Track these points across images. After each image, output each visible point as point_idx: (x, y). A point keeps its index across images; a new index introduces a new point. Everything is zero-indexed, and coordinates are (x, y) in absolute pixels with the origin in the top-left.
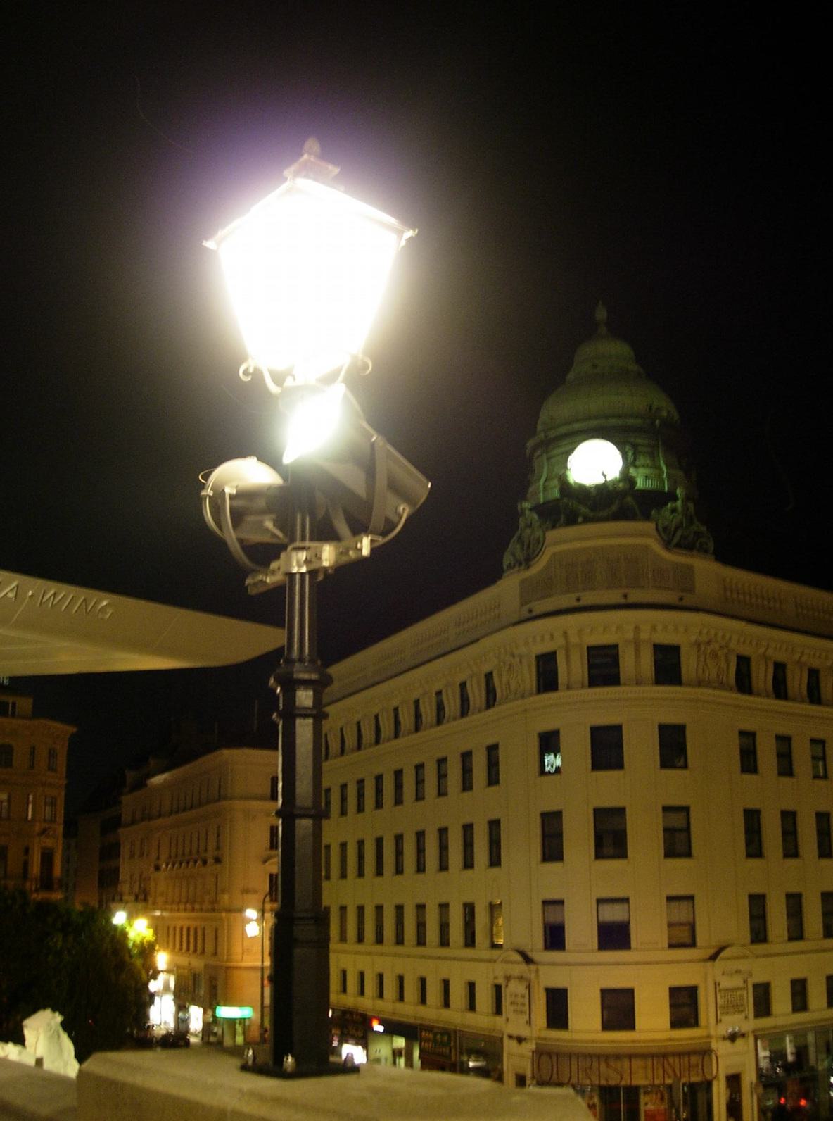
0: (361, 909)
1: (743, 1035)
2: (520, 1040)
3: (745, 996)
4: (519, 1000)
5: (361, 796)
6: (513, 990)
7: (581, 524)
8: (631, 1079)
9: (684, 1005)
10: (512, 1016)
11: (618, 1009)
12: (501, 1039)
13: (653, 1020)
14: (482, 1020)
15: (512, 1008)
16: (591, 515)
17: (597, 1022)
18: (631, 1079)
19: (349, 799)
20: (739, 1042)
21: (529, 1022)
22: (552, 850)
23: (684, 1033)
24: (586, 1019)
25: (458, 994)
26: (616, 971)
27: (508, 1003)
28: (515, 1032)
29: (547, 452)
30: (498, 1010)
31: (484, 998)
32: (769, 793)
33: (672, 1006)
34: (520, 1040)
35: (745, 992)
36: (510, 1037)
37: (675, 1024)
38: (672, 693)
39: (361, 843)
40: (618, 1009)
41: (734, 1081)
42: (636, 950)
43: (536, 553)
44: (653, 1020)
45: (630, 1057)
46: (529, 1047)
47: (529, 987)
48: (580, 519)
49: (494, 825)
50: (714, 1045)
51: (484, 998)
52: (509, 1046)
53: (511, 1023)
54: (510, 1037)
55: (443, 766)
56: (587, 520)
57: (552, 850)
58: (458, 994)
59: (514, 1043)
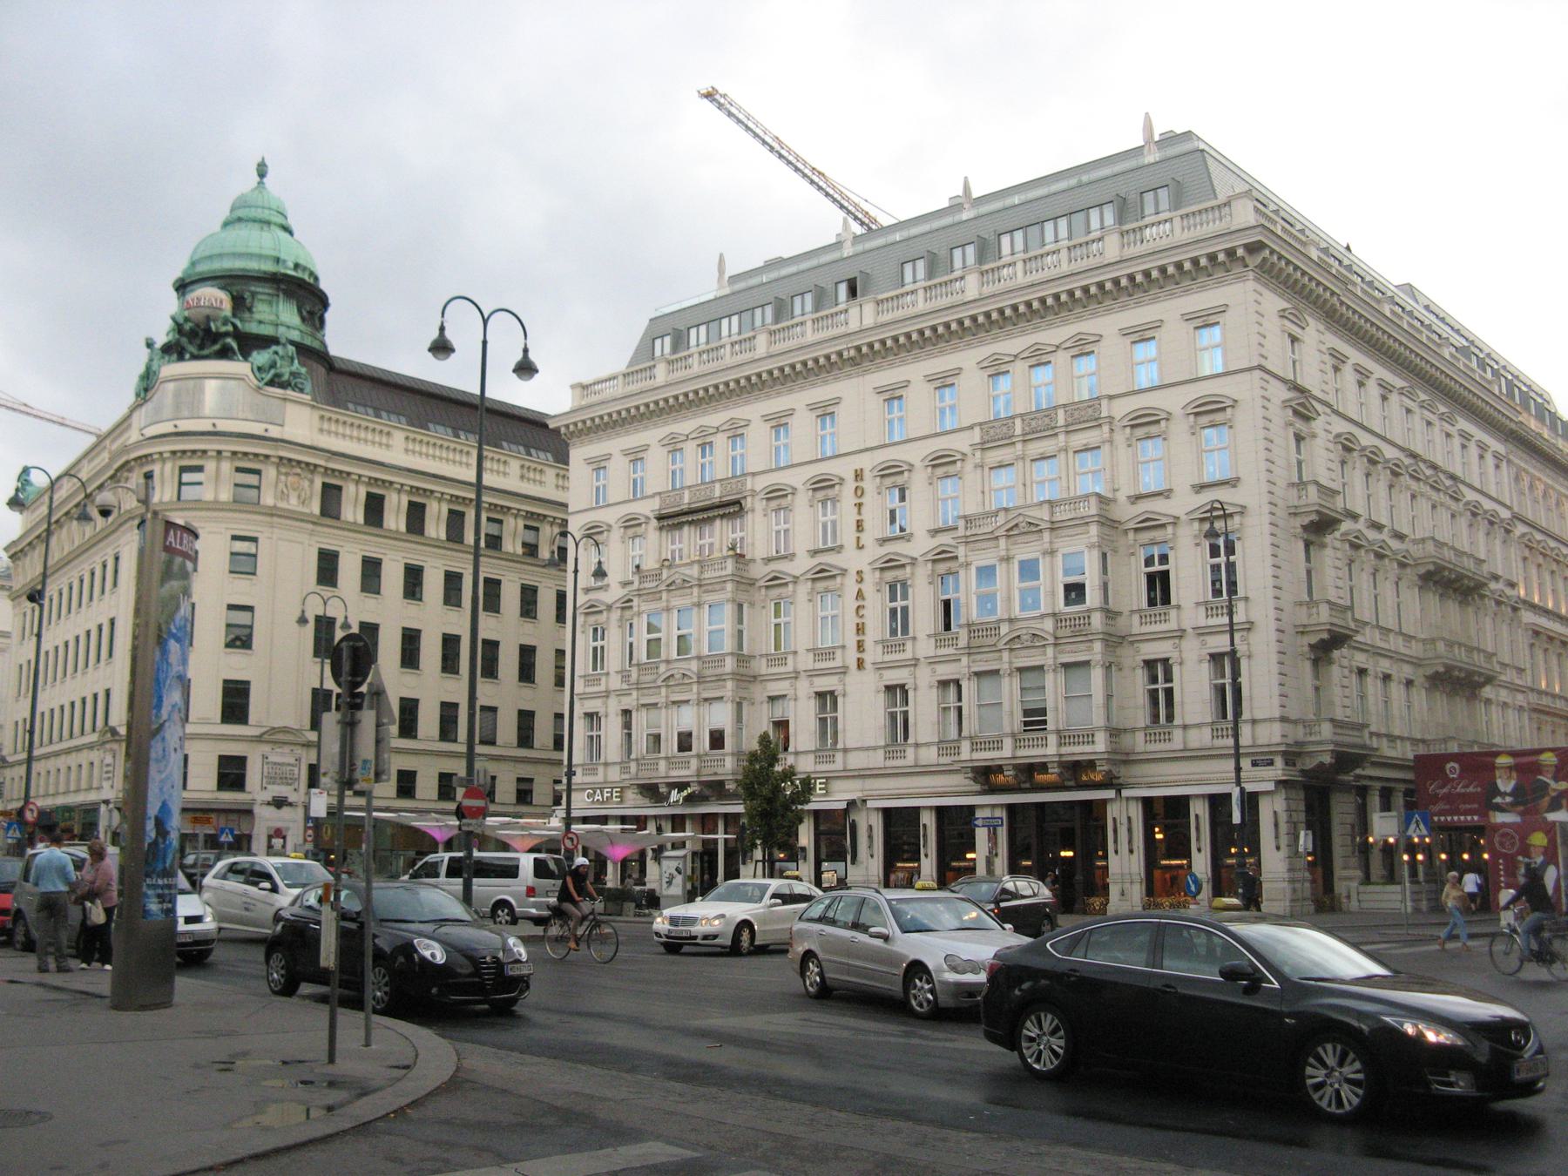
1: (290, 804)
17: (213, 782)
20: (285, 809)
56: (194, 357)
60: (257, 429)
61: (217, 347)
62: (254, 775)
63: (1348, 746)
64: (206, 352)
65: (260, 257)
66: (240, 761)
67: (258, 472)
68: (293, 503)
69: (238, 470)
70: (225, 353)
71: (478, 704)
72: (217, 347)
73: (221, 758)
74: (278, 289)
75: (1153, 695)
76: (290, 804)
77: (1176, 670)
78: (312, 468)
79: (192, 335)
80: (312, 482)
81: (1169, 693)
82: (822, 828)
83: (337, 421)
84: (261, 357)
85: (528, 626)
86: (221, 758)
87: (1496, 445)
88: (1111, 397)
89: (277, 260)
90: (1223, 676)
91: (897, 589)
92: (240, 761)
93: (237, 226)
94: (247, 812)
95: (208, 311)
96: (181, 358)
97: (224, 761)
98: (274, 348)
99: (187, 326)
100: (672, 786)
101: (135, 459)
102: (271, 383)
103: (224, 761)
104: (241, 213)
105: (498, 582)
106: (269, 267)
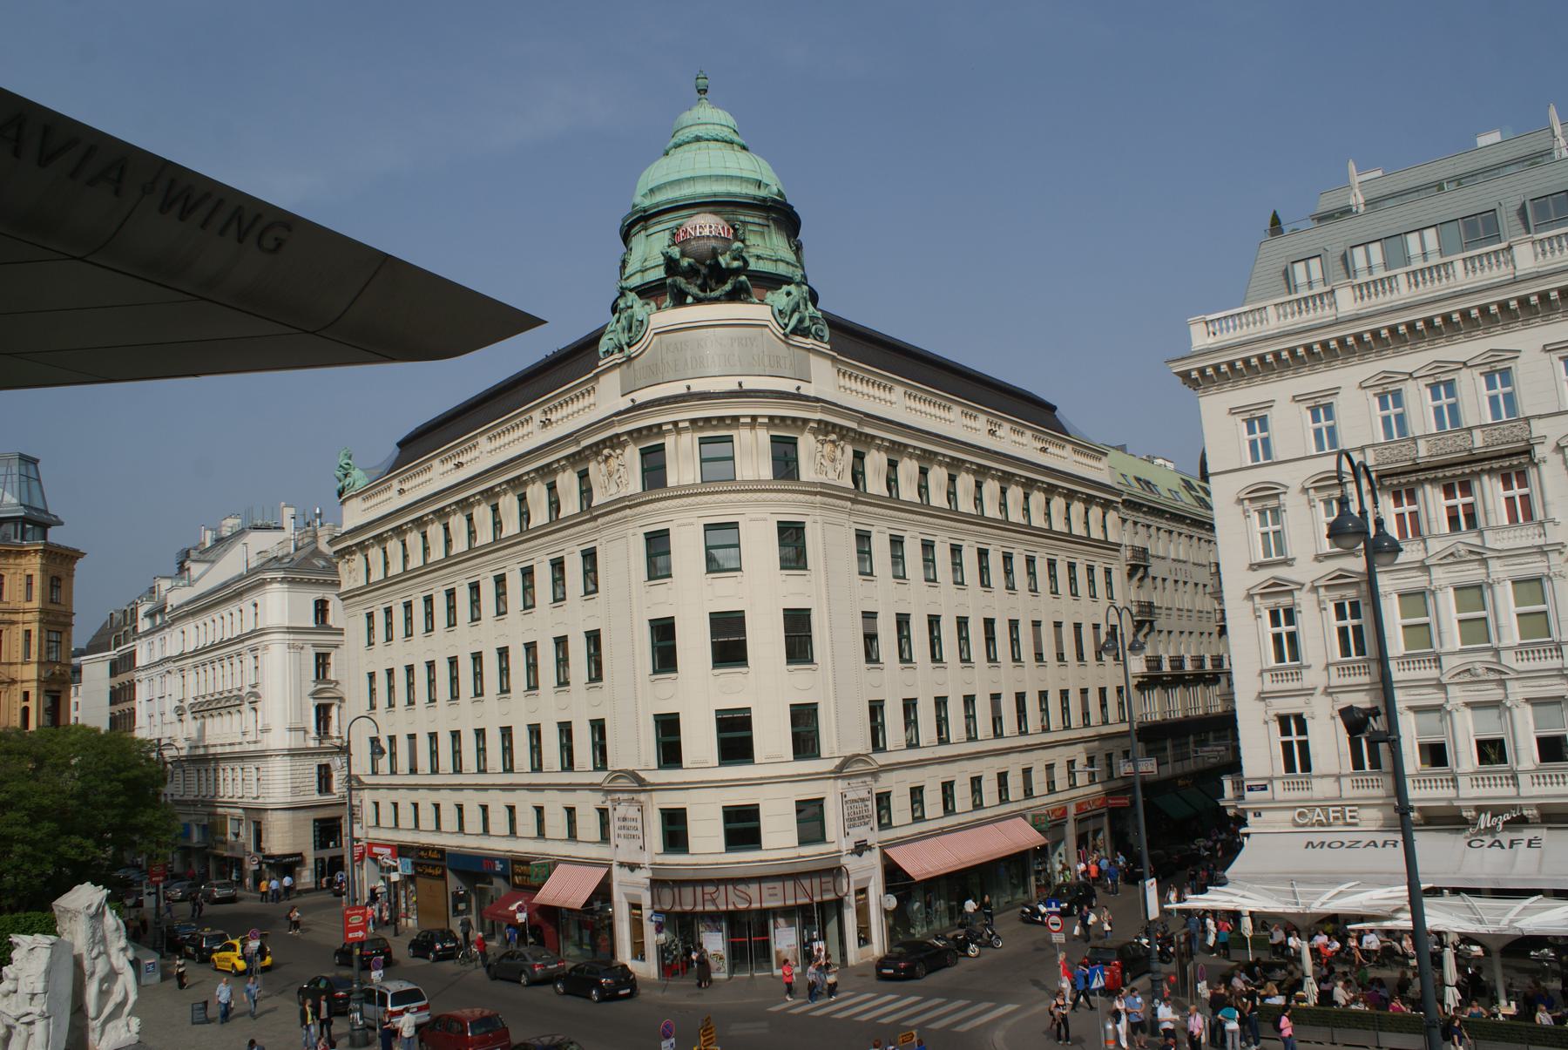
2: (633, 867)
6: (622, 811)
8: (1323, 776)
9: (810, 816)
10: (622, 842)
11: (742, 827)
13: (779, 836)
16: (702, 295)
17: (720, 842)
18: (1323, 776)
19: (1536, 172)
20: (866, 854)
21: (642, 848)
22: (665, 659)
23: (811, 850)
24: (708, 839)
26: (732, 689)
30: (605, 838)
31: (588, 825)
33: (799, 821)
34: (633, 867)
36: (622, 865)
37: (803, 842)
40: (742, 827)
43: (207, 577)
45: (760, 879)
46: (643, 876)
47: (641, 810)
48: (690, 300)
49: (594, 638)
50: (843, 861)
54: (622, 865)
56: (698, 301)
57: (665, 659)
60: (788, 386)
61: (728, 287)
63: (1541, 797)
65: (742, 179)
68: (831, 478)
69: (703, 441)
70: (735, 296)
72: (728, 287)
74: (767, 218)
75: (1287, 747)
77: (1310, 725)
79: (691, 273)
81: (1304, 746)
82: (143, 982)
84: (779, 299)
85: (801, 673)
87: (1165, 525)
88: (1540, 417)
89: (759, 184)
90: (1290, 734)
93: (695, 146)
95: (713, 243)
96: (680, 300)
97: (801, 806)
98: (785, 288)
99: (685, 262)
100: (1480, 810)
101: (630, 433)
102: (795, 331)
103: (801, 806)
106: (752, 190)
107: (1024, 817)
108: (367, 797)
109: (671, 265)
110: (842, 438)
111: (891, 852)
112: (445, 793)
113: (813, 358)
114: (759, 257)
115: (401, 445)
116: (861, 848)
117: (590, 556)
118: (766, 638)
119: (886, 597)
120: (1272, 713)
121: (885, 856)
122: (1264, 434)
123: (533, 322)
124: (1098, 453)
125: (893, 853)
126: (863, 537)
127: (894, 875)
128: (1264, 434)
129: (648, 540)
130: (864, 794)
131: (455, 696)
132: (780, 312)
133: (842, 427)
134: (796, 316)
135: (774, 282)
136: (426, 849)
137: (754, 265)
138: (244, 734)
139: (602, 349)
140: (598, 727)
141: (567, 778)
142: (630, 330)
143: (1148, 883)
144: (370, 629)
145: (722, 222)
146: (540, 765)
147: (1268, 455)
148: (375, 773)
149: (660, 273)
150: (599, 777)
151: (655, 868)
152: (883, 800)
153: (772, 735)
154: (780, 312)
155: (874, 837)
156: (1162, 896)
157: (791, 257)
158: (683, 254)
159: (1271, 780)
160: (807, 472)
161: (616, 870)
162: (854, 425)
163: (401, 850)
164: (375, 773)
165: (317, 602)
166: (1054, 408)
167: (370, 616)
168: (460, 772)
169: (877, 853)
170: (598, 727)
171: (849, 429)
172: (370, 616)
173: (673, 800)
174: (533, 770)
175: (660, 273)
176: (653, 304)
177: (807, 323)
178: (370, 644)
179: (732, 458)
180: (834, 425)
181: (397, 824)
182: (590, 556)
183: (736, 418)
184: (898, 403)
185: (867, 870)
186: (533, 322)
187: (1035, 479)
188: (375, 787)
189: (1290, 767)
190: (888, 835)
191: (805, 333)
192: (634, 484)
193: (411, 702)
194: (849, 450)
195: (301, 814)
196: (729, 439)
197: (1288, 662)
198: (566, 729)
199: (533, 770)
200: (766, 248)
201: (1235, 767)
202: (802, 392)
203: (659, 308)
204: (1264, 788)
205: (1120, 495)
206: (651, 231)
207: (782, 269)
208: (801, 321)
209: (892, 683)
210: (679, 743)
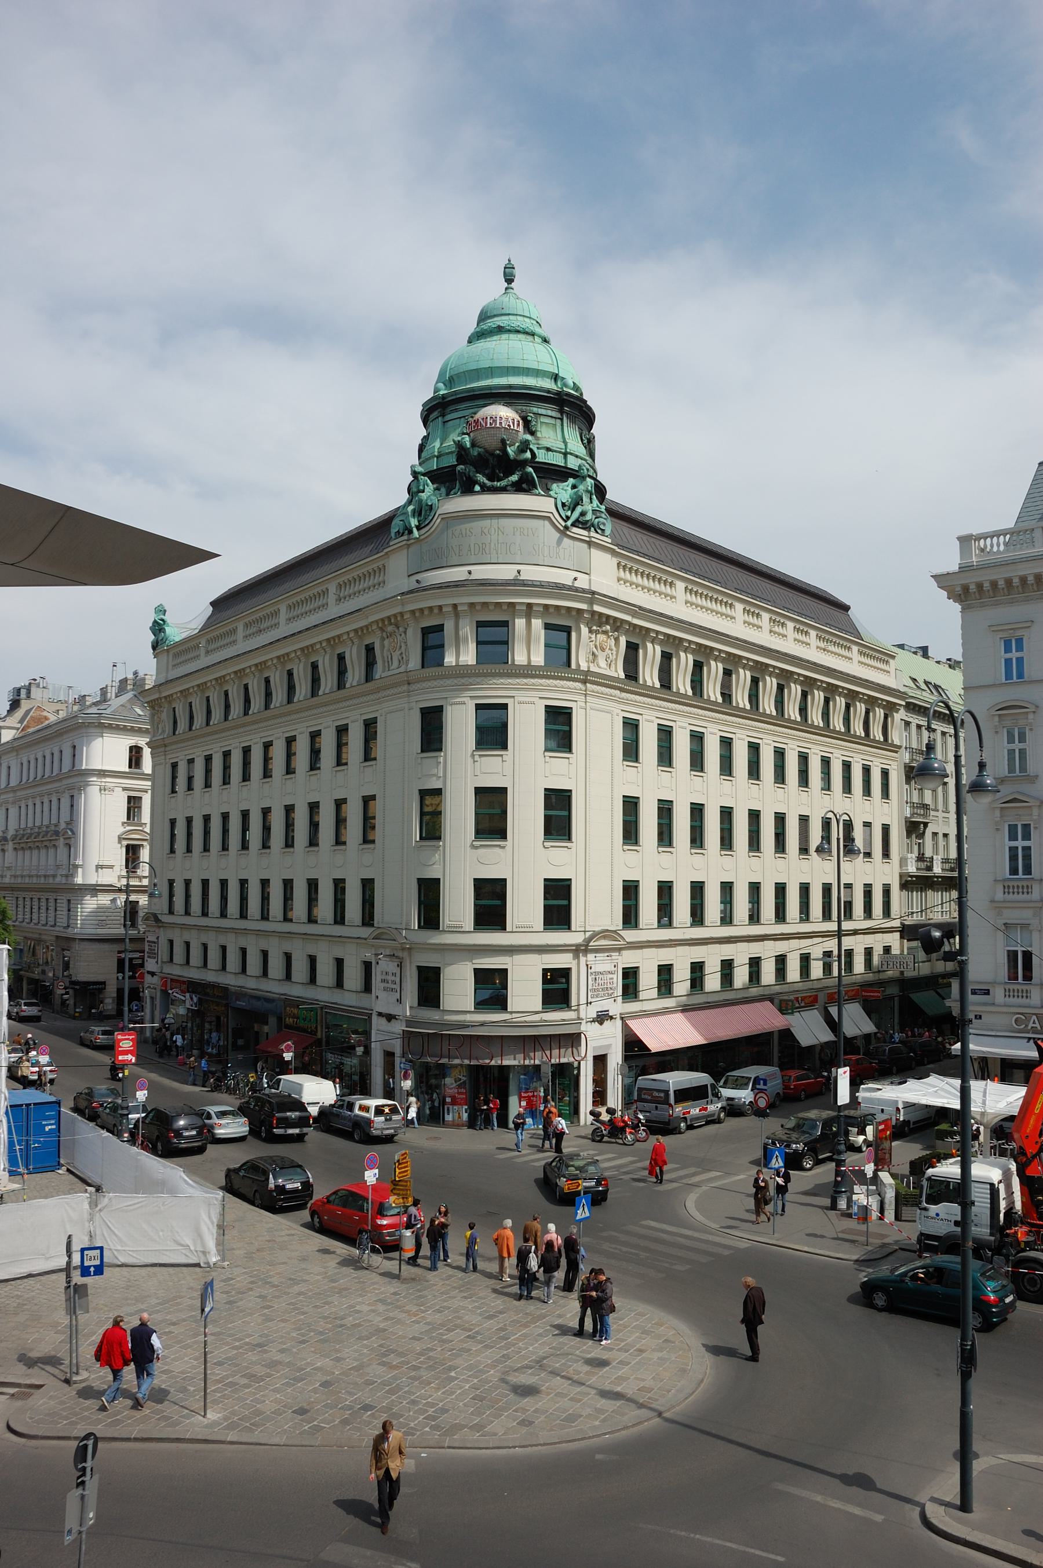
0: (224, 883)
1: (611, 1018)
3: (615, 980)
4: (390, 978)
5: (226, 767)
6: (384, 967)
7: (478, 493)
10: (382, 995)
12: (370, 1016)
13: (525, 994)
14: (349, 998)
15: (383, 985)
17: (537, 1003)
20: (607, 1023)
25: (326, 973)
27: (379, 978)
28: (384, 1010)
29: (443, 416)
30: (367, 988)
31: (353, 977)
32: (649, 783)
34: (390, 1018)
35: (615, 976)
36: (380, 1014)
38: (304, 1019)
39: (207, 819)
40: (492, 988)
41: (600, 1061)
42: (383, 345)
44: (525, 994)
46: (398, 1027)
48: (477, 488)
50: (583, 1028)
51: (353, 977)
52: (378, 1024)
53: (382, 1001)
55: (317, 739)
56: (485, 490)
57: (432, 828)
58: (326, 973)
59: (383, 1020)
61: (514, 478)
62: (579, 990)
64: (503, 483)
66: (564, 974)
67: (505, 624)
70: (524, 486)
71: (843, 948)
72: (514, 478)
73: (545, 971)
74: (562, 412)
76: (611, 1018)
78: (617, 625)
80: (617, 640)
83: (696, 593)
84: (563, 491)
86: (545, 971)
89: (556, 377)
91: (775, 633)
92: (564, 974)
94: (573, 1040)
96: (468, 489)
98: (571, 481)
99: (475, 452)
104: (484, 327)
105: (501, 793)
106: (548, 384)
107: (772, 1001)
108: (164, 936)
109: (462, 454)
110: (616, 629)
111: (632, 1024)
112: (194, 933)
113: (595, 553)
114: (548, 449)
115: (212, 604)
116: (602, 1018)
117: (370, 727)
118: (526, 815)
119: (649, 783)
120: (1000, 923)
121: (626, 1028)
122: (1019, 654)
123: (204, 556)
124: (883, 656)
125: (634, 1025)
126: (631, 727)
127: (633, 1046)
128: (1019, 654)
129: (422, 714)
130: (609, 967)
131: (206, 849)
132: (563, 505)
133: (615, 619)
134: (579, 509)
135: (561, 474)
136: (214, 986)
137: (542, 457)
138: (58, 867)
139: (393, 531)
140: (368, 884)
141: (338, 930)
142: (420, 515)
143: (841, 1071)
144: (174, 778)
145: (517, 417)
146: (343, 918)
147: (1020, 675)
148: (171, 912)
149: (452, 460)
150: (366, 932)
151: (409, 1023)
152: (630, 976)
153: (525, 907)
154: (563, 505)
155: (617, 1007)
156: (855, 1084)
157: (582, 451)
158: (473, 444)
159: (994, 983)
160: (581, 660)
161: (374, 1018)
162: (628, 618)
163: (192, 986)
164: (171, 912)
165: (131, 748)
166: (846, 608)
167: (174, 766)
168: (246, 918)
169: (619, 1022)
170: (368, 884)
171: (623, 621)
172: (174, 766)
173: (428, 960)
174: (336, 922)
175: (452, 460)
176: (443, 490)
177: (589, 516)
178: (173, 791)
179: (506, 643)
180: (608, 617)
181: (188, 962)
182: (370, 727)
183: (512, 605)
184: (678, 602)
185: (606, 1040)
186: (204, 556)
187: (813, 682)
188: (173, 925)
189: (1013, 977)
190: (633, 1007)
191: (585, 525)
192: (414, 661)
193: (189, 850)
194: (623, 640)
195: (106, 947)
196: (505, 624)
197: (1021, 875)
198: (339, 886)
199: (336, 922)
200: (555, 439)
201: (961, 973)
202: (577, 584)
203: (448, 494)
204: (987, 992)
205: (903, 699)
206: (448, 417)
207: (573, 463)
208: (583, 514)
209: (649, 864)
210: (624, 900)
